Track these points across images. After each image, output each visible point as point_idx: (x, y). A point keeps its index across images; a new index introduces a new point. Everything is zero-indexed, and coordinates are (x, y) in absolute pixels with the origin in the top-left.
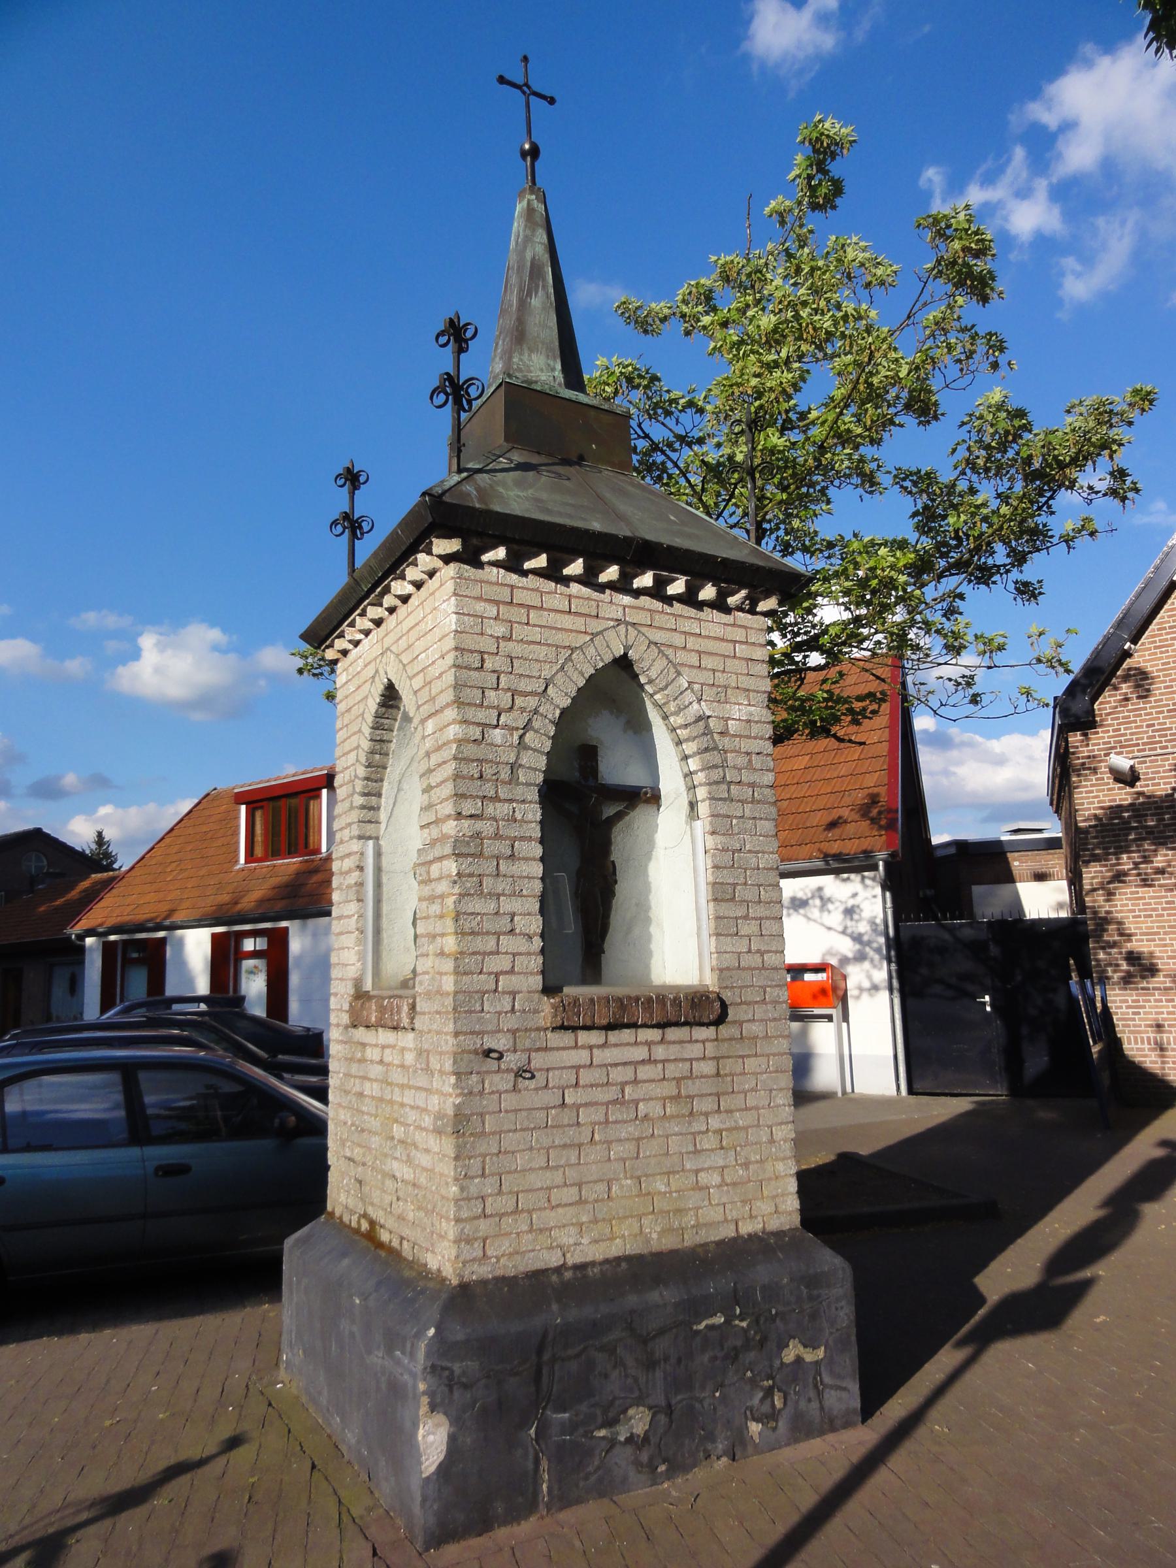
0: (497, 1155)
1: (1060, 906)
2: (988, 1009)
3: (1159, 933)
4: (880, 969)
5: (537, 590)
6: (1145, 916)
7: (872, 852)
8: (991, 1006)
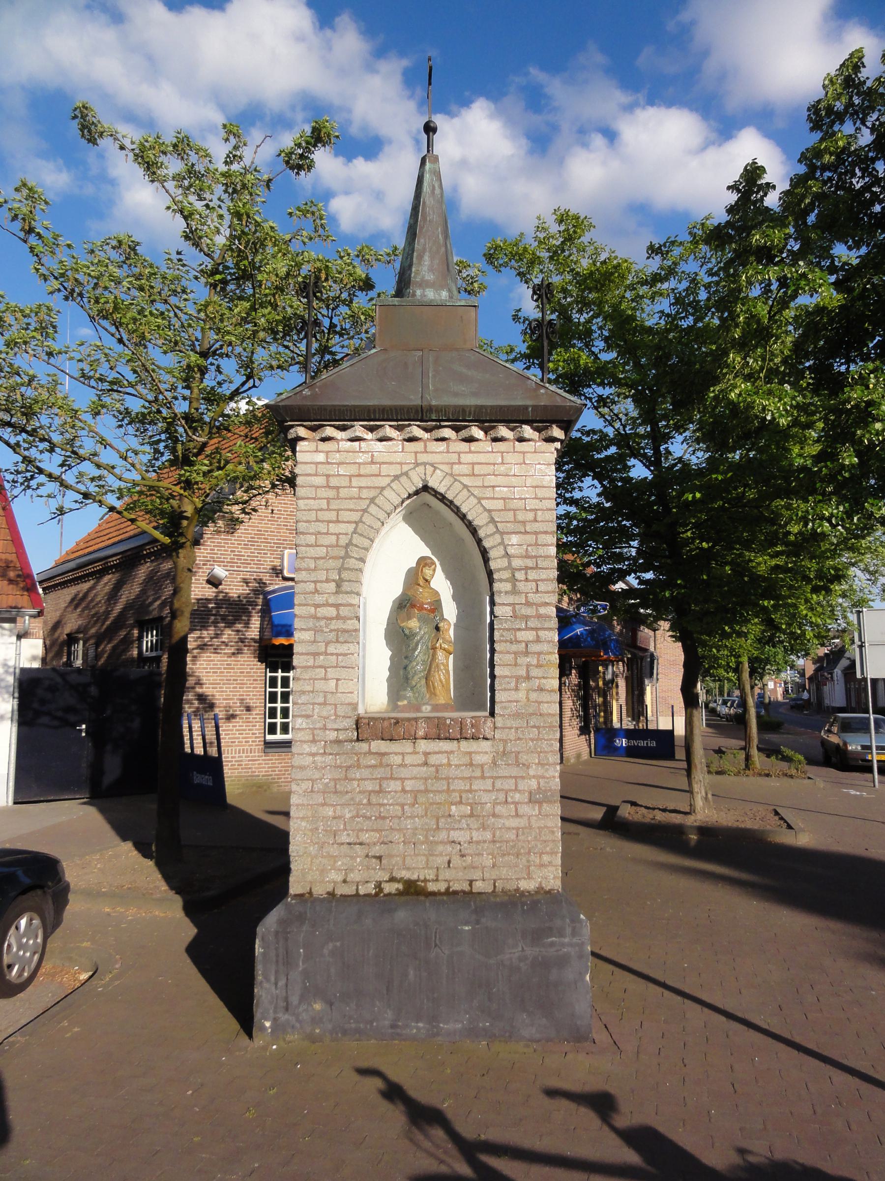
0: (413, 805)
1: (34, 658)
2: (84, 734)
3: (219, 684)
4: (8, 702)
5: (541, 499)
6: (214, 672)
7: (21, 608)
8: (86, 732)
